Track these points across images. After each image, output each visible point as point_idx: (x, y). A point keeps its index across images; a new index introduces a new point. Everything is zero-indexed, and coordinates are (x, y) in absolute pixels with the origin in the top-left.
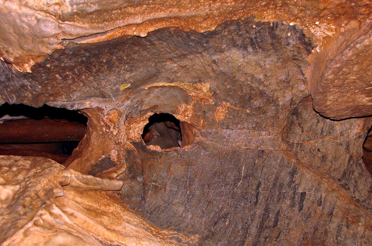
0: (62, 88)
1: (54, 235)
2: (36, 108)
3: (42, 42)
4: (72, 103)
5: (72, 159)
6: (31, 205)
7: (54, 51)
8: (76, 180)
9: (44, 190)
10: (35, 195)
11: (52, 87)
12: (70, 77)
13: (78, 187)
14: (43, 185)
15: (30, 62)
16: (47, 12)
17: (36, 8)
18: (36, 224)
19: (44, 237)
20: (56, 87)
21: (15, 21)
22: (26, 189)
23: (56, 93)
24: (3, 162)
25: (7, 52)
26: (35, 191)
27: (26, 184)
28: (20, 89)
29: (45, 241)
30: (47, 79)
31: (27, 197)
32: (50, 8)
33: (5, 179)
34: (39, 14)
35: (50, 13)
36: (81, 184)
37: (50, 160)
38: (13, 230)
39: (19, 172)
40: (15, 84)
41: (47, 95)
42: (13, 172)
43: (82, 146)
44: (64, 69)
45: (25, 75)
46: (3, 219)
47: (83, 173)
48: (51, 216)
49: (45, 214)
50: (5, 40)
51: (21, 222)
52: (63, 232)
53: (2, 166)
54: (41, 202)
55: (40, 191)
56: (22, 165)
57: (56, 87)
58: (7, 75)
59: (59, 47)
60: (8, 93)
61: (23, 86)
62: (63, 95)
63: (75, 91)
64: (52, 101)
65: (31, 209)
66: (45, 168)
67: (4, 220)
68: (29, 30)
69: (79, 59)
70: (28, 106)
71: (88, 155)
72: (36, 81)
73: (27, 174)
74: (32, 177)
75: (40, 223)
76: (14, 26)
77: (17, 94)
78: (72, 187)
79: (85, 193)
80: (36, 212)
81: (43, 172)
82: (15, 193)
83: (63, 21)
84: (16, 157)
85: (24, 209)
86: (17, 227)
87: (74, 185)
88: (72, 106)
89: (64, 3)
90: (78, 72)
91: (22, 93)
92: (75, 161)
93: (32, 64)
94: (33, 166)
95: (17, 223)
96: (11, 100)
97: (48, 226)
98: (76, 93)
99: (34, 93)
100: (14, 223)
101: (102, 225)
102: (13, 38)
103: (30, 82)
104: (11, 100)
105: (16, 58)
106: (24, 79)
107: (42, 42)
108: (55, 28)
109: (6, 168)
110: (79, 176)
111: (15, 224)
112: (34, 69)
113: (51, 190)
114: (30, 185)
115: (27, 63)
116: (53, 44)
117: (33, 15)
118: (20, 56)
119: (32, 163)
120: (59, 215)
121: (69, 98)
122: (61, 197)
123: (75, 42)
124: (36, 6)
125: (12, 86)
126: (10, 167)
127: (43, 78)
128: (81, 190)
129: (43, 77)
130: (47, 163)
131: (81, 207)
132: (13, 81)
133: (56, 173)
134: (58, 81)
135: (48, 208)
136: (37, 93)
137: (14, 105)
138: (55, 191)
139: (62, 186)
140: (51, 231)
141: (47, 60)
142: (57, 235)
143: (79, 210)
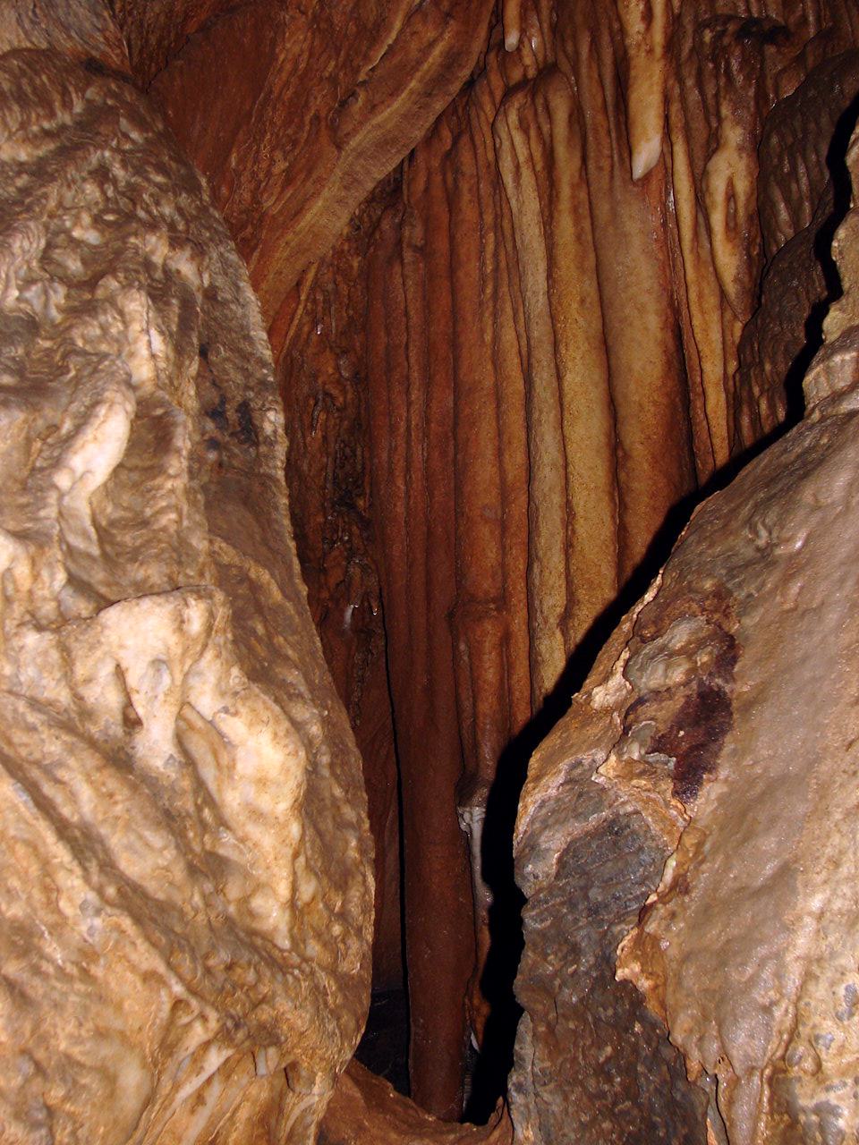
0: (575, 1059)
1: (144, 1057)
2: (512, 984)
3: (706, 1018)
4: (531, 1088)
5: (360, 1078)
6: (234, 988)
7: (681, 1050)
8: (303, 1105)
9: (276, 1020)
10: (261, 997)
11: (574, 1031)
12: (606, 1087)
13: (281, 1110)
14: (289, 1016)
15: (647, 978)
16: (794, 1033)
17: (802, 1004)
18: (178, 1004)
19: (140, 1029)
20: (576, 1045)
21: (761, 942)
22: (279, 966)
23: (557, 1042)
24: (358, 894)
25: (673, 915)
26: (274, 994)
27: (293, 967)
28: (566, 940)
29: (128, 1033)
30: (597, 1020)
31: (257, 972)
32: (806, 1044)
33: (308, 904)
34: (787, 1011)
35: (792, 1045)
36: (290, 1123)
37: (363, 1030)
38: (164, 940)
39: (328, 944)
40: (581, 928)
41: (552, 1016)
42: (327, 926)
43: (400, 1109)
44: (629, 1071)
45: (607, 963)
46: (197, 911)
47: (320, 1125)
48: (201, 1045)
49: (206, 1029)
50: (705, 911)
51: (186, 963)
52: (153, 1083)
53: (344, 893)
54: (241, 1014)
55: (274, 1010)
56: (348, 948)
57: (576, 1045)
58: (607, 906)
59: (694, 1065)
60: (553, 906)
61: (575, 951)
62: (552, 1061)
63: (566, 1099)
64: (534, 1029)
65: (223, 988)
66: (338, 1019)
67: (193, 913)
68: (739, 983)
69: (660, 1117)
70: (519, 961)
71: (375, 1131)
72: (592, 990)
73: (323, 968)
74: (312, 985)
75: (180, 1017)
76: (747, 941)
77: (553, 932)
78: (282, 1096)
79: (261, 1130)
80: (213, 1004)
81: (326, 1013)
82: (267, 937)
83: (771, 1081)
84: (371, 929)
85: (222, 967)
86: (172, 953)
87: (288, 1101)
88: (520, 1088)
89: (823, 1086)
90: (621, 1112)
91: (556, 947)
92: (356, 1089)
93: (639, 984)
94: (344, 982)
95: (183, 951)
96: (534, 913)
97: (172, 1037)
98: (558, 1101)
99: (557, 982)
100: (183, 942)
101: (19, 780)
102: (715, 934)
103: (586, 973)
104: (534, 913)
105: (655, 940)
106: (596, 957)
107: (706, 1018)
108: (747, 1056)
109: (339, 904)
110: (314, 1113)
111: (179, 943)
112: (625, 987)
113: (275, 1041)
114: (290, 978)
115: (642, 971)
116: (700, 1049)
117: (782, 995)
118: (662, 953)
119: (352, 977)
120: (202, 1068)
121: (541, 1079)
122: (252, 1067)
123: (710, 1112)
124: (808, 1004)
125: (576, 921)
126: (343, 916)
127: (601, 1009)
128: (273, 1121)
129: (605, 1010)
130: (352, 1025)
131: (221, 1123)
132: (590, 924)
133: (322, 1042)
134: (592, 1052)
135: (223, 1037)
136: (557, 990)
137: (521, 921)
138: (272, 1051)
139: (285, 1069)
140: (156, 1047)
141: (654, 1026)
142: (144, 1066)
143: (212, 1122)
